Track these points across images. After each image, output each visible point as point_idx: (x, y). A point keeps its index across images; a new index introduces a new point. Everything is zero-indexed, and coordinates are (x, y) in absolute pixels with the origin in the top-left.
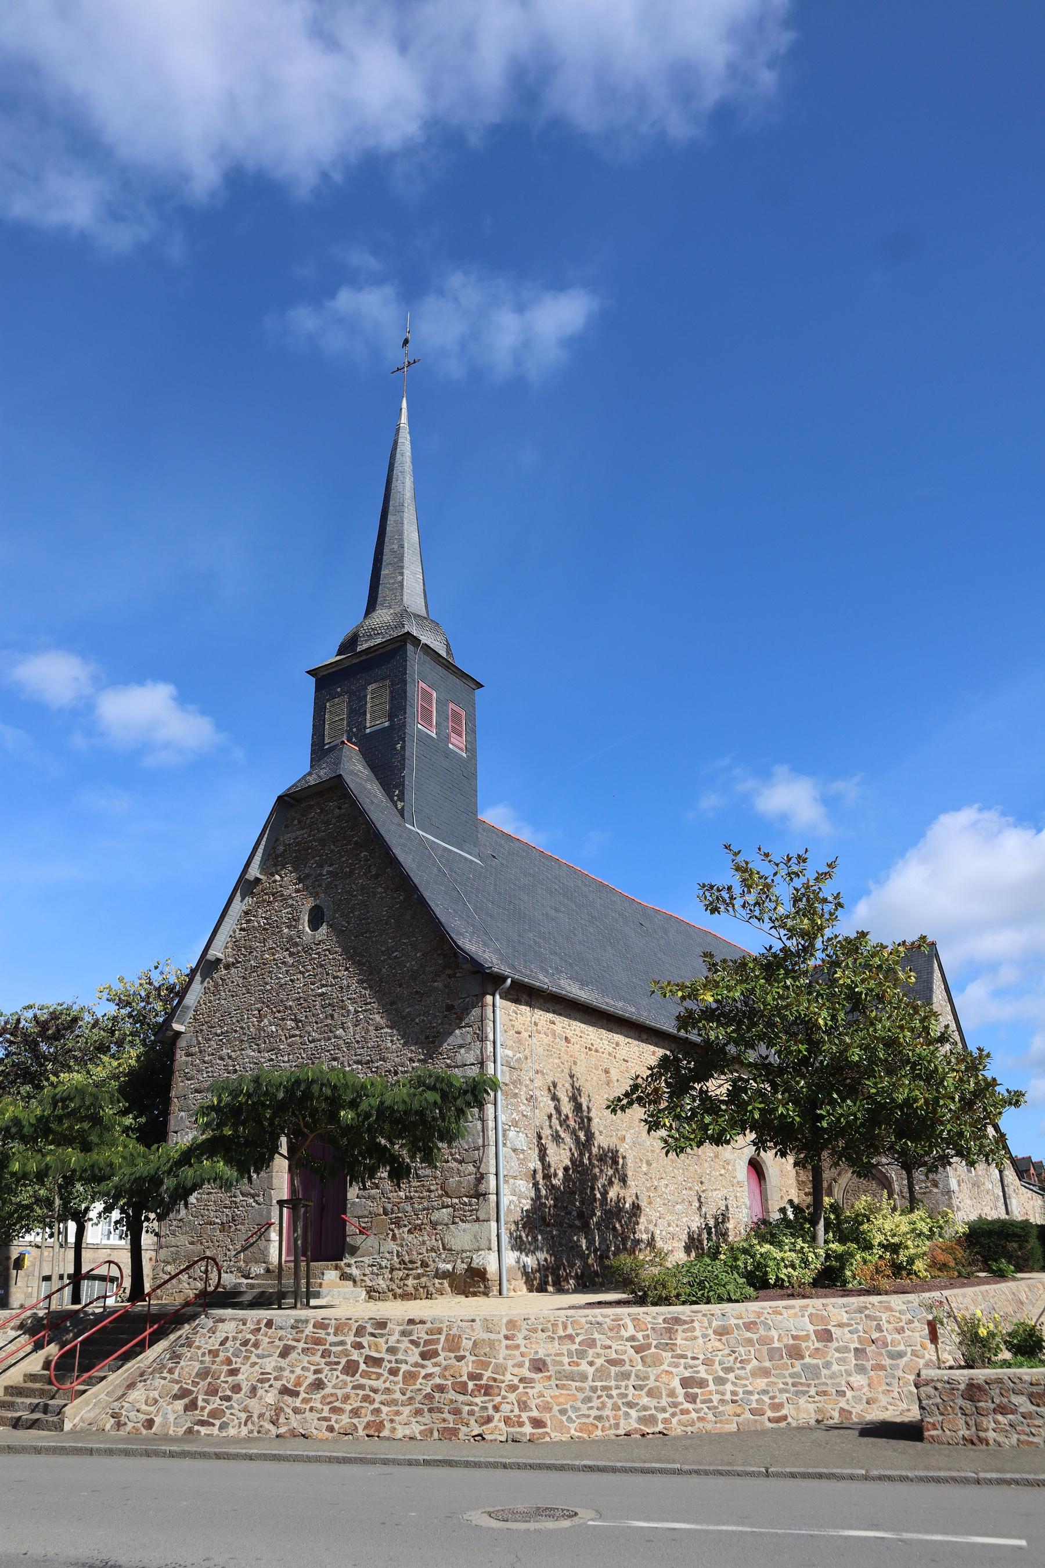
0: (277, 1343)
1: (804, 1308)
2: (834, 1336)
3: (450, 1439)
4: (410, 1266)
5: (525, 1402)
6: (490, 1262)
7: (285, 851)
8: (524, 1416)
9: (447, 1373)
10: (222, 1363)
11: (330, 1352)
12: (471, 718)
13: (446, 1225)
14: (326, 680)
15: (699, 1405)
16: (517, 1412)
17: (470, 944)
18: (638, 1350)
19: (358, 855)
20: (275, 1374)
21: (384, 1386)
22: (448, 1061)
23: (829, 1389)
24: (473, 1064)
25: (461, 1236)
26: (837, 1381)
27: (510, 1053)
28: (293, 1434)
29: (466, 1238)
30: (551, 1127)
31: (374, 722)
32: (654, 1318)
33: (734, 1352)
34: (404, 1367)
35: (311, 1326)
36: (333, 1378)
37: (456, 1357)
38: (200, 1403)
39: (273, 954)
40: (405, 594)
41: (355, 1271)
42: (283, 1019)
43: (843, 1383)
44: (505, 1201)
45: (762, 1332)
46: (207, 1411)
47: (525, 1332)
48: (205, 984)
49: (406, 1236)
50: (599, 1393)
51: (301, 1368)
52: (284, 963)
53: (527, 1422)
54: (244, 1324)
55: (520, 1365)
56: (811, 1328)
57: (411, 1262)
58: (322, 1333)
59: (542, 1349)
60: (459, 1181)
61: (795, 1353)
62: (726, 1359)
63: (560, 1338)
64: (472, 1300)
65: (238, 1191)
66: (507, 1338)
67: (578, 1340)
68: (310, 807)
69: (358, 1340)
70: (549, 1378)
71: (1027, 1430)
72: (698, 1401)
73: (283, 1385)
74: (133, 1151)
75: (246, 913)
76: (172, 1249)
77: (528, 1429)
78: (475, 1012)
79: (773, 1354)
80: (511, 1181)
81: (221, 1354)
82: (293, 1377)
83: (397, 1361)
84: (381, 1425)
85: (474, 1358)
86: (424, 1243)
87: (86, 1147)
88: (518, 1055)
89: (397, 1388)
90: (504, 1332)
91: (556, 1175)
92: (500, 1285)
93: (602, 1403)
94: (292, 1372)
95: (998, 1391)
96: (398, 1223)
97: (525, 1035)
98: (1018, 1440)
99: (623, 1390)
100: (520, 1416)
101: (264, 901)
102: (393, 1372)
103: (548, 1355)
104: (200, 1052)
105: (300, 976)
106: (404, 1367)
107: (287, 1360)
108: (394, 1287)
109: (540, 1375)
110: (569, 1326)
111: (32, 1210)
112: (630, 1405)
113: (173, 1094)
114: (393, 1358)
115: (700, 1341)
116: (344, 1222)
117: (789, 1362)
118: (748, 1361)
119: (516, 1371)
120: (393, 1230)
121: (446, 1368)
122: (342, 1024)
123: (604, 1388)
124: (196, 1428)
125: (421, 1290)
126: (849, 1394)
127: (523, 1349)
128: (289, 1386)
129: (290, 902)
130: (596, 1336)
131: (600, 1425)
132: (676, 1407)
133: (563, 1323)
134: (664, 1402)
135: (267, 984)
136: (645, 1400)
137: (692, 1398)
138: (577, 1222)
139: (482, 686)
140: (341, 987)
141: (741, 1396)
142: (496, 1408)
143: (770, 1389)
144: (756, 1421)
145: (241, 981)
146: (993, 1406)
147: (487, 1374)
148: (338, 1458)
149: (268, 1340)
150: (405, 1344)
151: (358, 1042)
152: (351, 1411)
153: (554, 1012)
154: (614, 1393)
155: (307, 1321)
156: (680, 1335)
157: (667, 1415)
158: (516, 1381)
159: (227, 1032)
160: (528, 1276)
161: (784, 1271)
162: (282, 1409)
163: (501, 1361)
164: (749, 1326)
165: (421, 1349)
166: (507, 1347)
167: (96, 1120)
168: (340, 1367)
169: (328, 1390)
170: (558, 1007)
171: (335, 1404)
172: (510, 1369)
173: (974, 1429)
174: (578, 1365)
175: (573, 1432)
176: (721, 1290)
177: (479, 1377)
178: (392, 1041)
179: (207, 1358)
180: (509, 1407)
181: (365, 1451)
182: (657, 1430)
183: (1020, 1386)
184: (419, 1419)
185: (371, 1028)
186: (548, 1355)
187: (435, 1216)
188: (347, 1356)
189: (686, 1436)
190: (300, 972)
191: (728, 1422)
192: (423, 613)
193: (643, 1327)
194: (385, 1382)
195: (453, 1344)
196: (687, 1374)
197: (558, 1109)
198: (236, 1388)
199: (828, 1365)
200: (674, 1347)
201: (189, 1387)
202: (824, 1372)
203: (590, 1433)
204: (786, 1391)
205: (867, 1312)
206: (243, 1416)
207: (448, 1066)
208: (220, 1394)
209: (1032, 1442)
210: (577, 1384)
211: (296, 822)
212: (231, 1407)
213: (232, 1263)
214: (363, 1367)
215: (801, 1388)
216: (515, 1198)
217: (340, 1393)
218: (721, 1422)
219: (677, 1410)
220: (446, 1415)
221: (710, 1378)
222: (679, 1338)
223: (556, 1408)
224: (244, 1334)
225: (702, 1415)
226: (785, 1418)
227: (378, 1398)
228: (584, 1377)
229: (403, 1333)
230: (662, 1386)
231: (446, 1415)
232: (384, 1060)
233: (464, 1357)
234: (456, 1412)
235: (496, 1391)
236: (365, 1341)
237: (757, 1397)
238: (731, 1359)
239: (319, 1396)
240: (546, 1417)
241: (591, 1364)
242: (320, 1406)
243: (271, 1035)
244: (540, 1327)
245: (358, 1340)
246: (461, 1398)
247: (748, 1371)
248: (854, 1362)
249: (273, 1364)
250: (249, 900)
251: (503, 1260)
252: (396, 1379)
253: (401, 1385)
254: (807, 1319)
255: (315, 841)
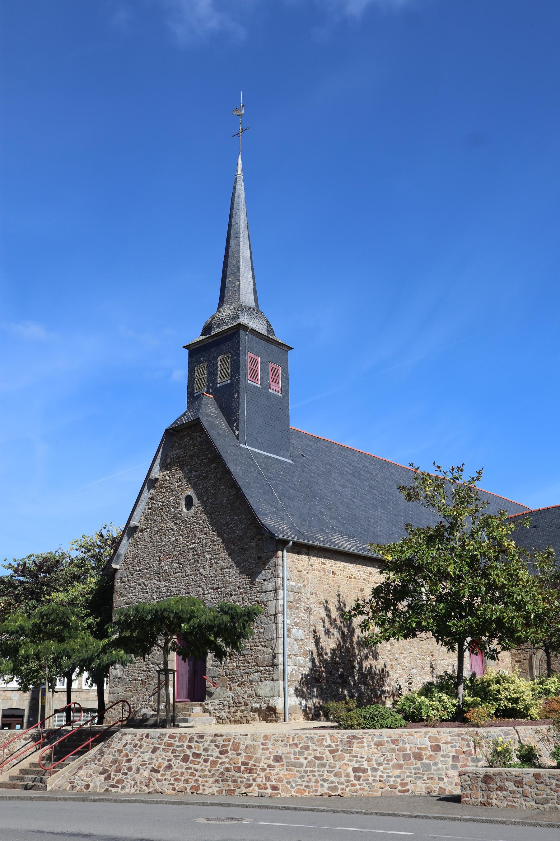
0: (151, 746)
1: (426, 733)
2: (442, 748)
3: (231, 795)
4: (238, 705)
5: (269, 777)
6: (279, 704)
7: (171, 462)
8: (268, 784)
9: (231, 762)
10: (124, 756)
11: (176, 750)
12: (285, 370)
13: (257, 682)
14: (195, 352)
15: (361, 782)
16: (264, 782)
17: (269, 521)
18: (331, 752)
19: (210, 466)
20: (149, 762)
21: (201, 768)
22: (258, 589)
23: (434, 777)
24: (271, 591)
25: (264, 689)
26: (440, 772)
27: (294, 584)
28: (156, 792)
29: (267, 690)
30: (324, 627)
31: (222, 380)
32: (342, 736)
33: (384, 755)
34: (211, 758)
35: (167, 737)
36: (177, 764)
37: (236, 753)
38: (112, 776)
39: (166, 524)
40: (241, 293)
41: (210, 708)
42: (172, 563)
43: (444, 774)
44: (289, 669)
45: (401, 745)
46: (115, 780)
47: (272, 741)
48: (130, 541)
49: (236, 688)
50: (309, 773)
51: (161, 758)
52: (172, 529)
53: (269, 787)
54: (135, 736)
55: (268, 758)
56: (429, 744)
57: (239, 703)
58: (172, 741)
59: (281, 750)
60: (264, 658)
61: (418, 757)
62: (379, 759)
63: (290, 745)
64: (269, 724)
65: (150, 662)
66: (263, 744)
67: (300, 746)
68: (184, 435)
69: (190, 744)
70: (283, 765)
71: (512, 799)
72: (361, 780)
73: (152, 767)
74: (86, 642)
75: (151, 499)
76: (116, 695)
77: (269, 791)
78: (273, 561)
79: (406, 757)
80: (294, 657)
81: (123, 751)
82: (157, 763)
83: (208, 755)
84: (198, 788)
85: (246, 754)
86: (246, 692)
87: (62, 640)
88: (299, 585)
89: (207, 769)
90: (262, 741)
91: (326, 654)
92: (285, 716)
93: (309, 779)
94: (157, 760)
95: (499, 779)
96: (232, 680)
97: (304, 572)
98: (507, 804)
99: (321, 773)
100: (266, 784)
101: (160, 492)
102: (206, 761)
103: (283, 754)
104: (128, 581)
105: (180, 537)
106: (211, 758)
107: (155, 754)
108: (230, 717)
109: (278, 764)
110: (296, 738)
111: (39, 673)
112: (324, 780)
113: (114, 605)
114: (206, 754)
115: (366, 748)
116: (205, 680)
117: (414, 761)
118: (391, 760)
119: (266, 761)
120: (230, 685)
121: (231, 759)
122: (203, 566)
123: (311, 771)
124: (110, 788)
125: (244, 718)
126: (446, 780)
127: (270, 750)
128: (155, 768)
129: (175, 493)
130: (310, 744)
131: (307, 790)
132: (349, 782)
133: (293, 737)
134: (342, 780)
135: (163, 541)
136: (333, 778)
137: (358, 778)
138: (338, 680)
139: (292, 349)
140: (202, 544)
141: (385, 778)
142: (254, 780)
143: (402, 775)
144: (391, 791)
145: (149, 539)
146: (496, 787)
147: (251, 762)
148: (170, 802)
149: (146, 744)
150: (212, 746)
151: (211, 577)
152: (184, 780)
153: (325, 557)
154: (316, 774)
155: (165, 735)
156: (355, 745)
157: (343, 786)
158: (265, 767)
159: (142, 569)
160: (305, 710)
161: (432, 712)
162: (151, 779)
163: (259, 756)
164: (394, 742)
165: (220, 749)
166: (262, 749)
167: (66, 625)
168: (180, 758)
169: (174, 770)
170: (327, 555)
171: (177, 777)
172: (263, 760)
173: (486, 798)
174: (298, 759)
175: (293, 793)
176: (383, 722)
177: (247, 764)
178: (229, 576)
179: (117, 754)
180: (261, 779)
181: (190, 799)
182: (337, 794)
183: (510, 777)
184: (217, 784)
185: (218, 569)
186: (283, 754)
187: (252, 677)
188: (184, 752)
189: (352, 797)
190: (181, 535)
191: (376, 791)
192: (253, 305)
193: (336, 740)
194: (201, 766)
195: (236, 747)
196: (357, 766)
197: (329, 616)
198: (130, 769)
199: (436, 764)
200: (351, 751)
201: (107, 768)
202: (433, 767)
203: (302, 794)
204: (410, 777)
205: (463, 736)
206: (133, 782)
207: (259, 592)
208: (122, 772)
209: (513, 806)
210: (297, 769)
211: (177, 444)
212: (127, 778)
213: (147, 703)
214: (191, 758)
215: (419, 775)
216: (296, 667)
217: (179, 771)
218: (372, 791)
219: (349, 784)
220: (230, 783)
221: (369, 768)
222: (354, 747)
223: (285, 781)
224: (135, 741)
225: (362, 787)
226: (408, 791)
227: (198, 774)
228: (301, 765)
229: (212, 741)
230: (343, 771)
231: (230, 783)
232: (225, 587)
233: (240, 754)
234: (235, 781)
235: (255, 771)
236: (193, 745)
237: (394, 779)
238: (382, 758)
239: (170, 772)
240: (280, 785)
241: (306, 758)
242: (169, 778)
243: (165, 572)
244: (280, 739)
245: (190, 744)
246: (238, 774)
247: (390, 765)
248: (451, 763)
249: (148, 756)
250: (152, 491)
251: (289, 701)
252: (207, 764)
253: (209, 768)
254: (427, 739)
255: (187, 456)
